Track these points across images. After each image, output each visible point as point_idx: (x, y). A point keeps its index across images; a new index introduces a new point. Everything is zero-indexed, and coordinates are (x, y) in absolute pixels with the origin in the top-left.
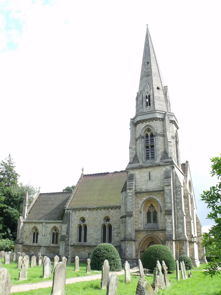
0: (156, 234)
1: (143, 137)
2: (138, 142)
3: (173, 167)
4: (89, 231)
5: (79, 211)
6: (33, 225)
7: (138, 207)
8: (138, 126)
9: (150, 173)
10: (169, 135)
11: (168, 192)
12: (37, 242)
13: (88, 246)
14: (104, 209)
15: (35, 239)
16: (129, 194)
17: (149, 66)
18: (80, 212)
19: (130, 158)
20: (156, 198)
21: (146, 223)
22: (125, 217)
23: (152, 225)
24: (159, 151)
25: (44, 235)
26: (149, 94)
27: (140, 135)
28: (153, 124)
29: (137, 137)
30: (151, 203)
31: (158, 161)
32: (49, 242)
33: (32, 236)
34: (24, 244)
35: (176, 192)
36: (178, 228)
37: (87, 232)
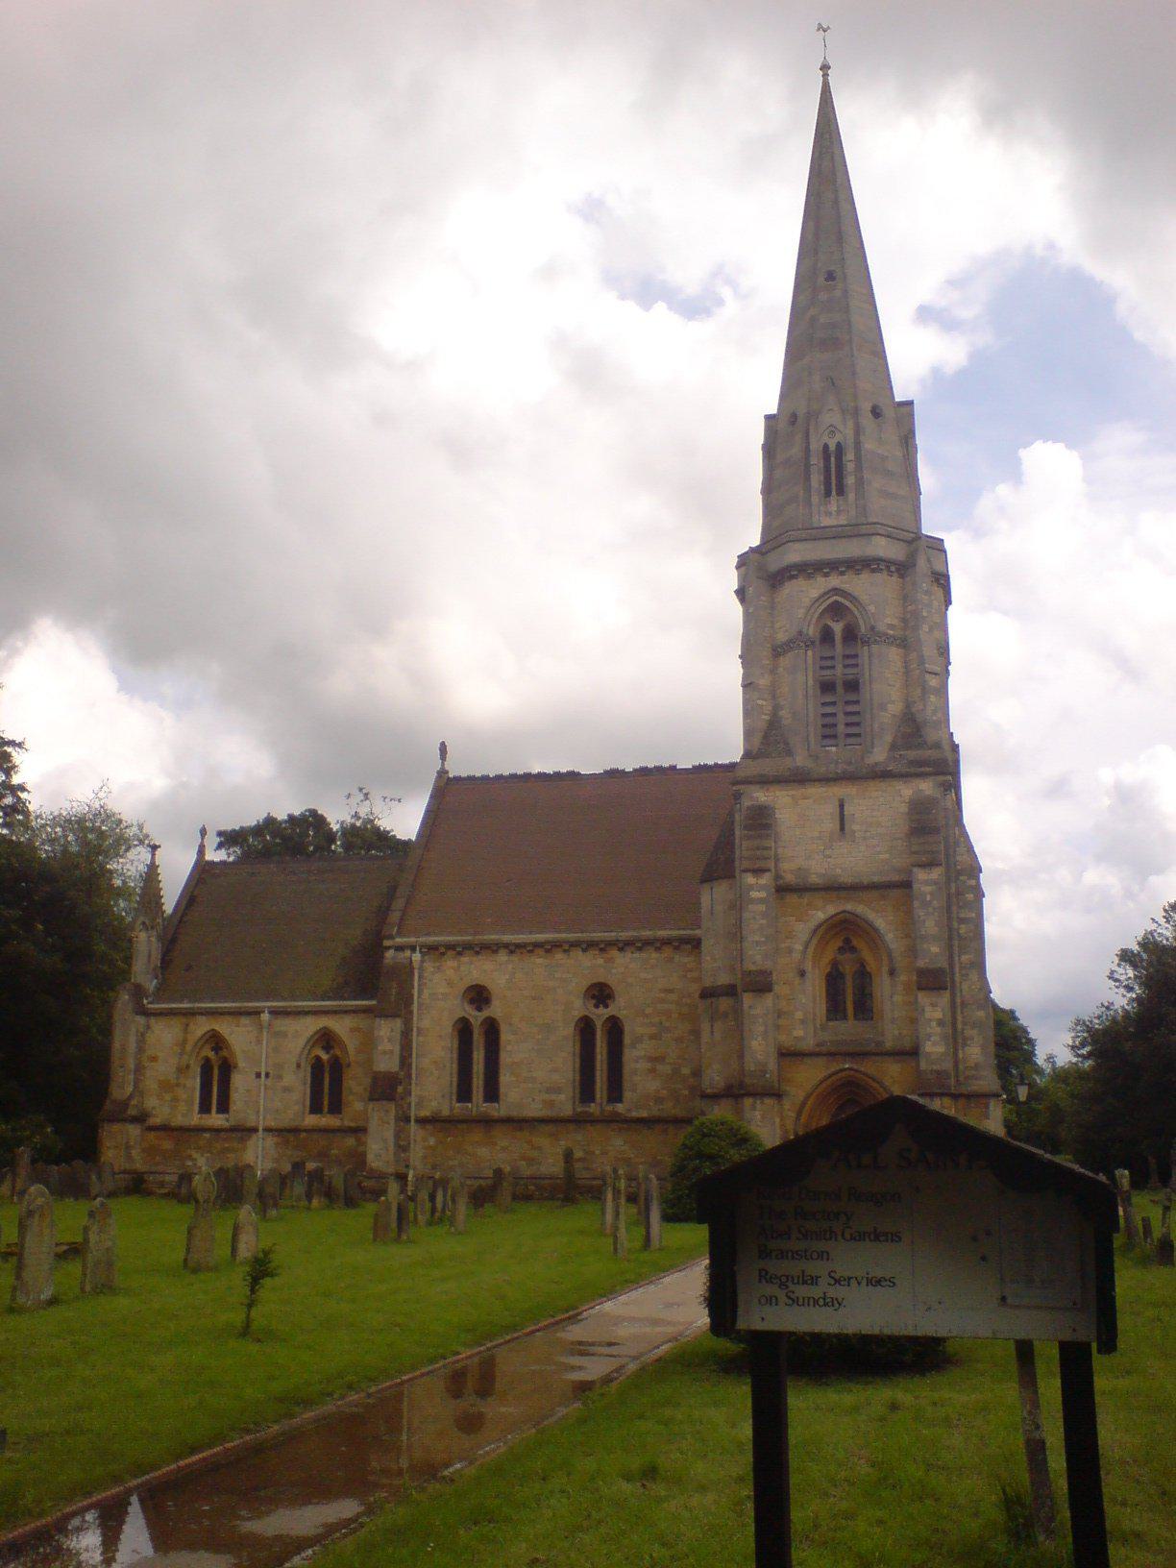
0: (869, 1067)
1: (809, 644)
2: (785, 661)
4: (514, 1050)
5: (460, 954)
7: (790, 951)
8: (789, 589)
9: (842, 806)
11: (931, 894)
12: (224, 1107)
13: (508, 1121)
14: (584, 950)
15: (210, 1092)
16: (754, 894)
17: (838, 293)
18: (465, 959)
19: (748, 734)
20: (871, 915)
21: (825, 1018)
22: (731, 991)
23: (848, 1029)
24: (886, 710)
25: (267, 1075)
26: (838, 438)
27: (800, 633)
28: (861, 585)
29: (782, 637)
30: (846, 931)
31: (879, 755)
32: (296, 1107)
33: (194, 1078)
34: (152, 1121)
35: (959, 893)
36: (965, 1045)
37: (503, 1055)
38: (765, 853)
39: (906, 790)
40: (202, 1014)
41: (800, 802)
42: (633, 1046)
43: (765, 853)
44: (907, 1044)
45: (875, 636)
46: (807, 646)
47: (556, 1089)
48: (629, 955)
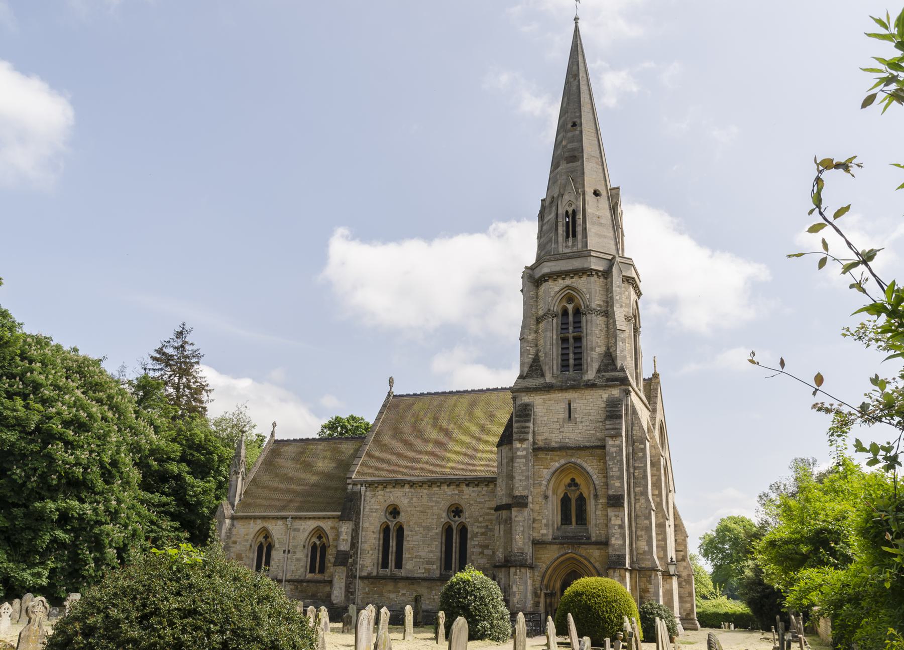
0: (583, 551)
1: (555, 315)
2: (541, 326)
3: (628, 393)
4: (411, 541)
6: (258, 525)
7: (540, 485)
8: (544, 287)
9: (570, 405)
10: (620, 314)
13: (407, 578)
16: (519, 453)
20: (585, 465)
22: (508, 507)
25: (289, 552)
26: (573, 207)
27: (549, 310)
28: (581, 283)
29: (541, 313)
36: (637, 539)
38: (526, 430)
39: (605, 395)
40: (259, 518)
41: (547, 402)
42: (472, 539)
43: (526, 430)
44: (603, 540)
45: (590, 311)
46: (553, 317)
47: (429, 562)
48: (471, 488)
